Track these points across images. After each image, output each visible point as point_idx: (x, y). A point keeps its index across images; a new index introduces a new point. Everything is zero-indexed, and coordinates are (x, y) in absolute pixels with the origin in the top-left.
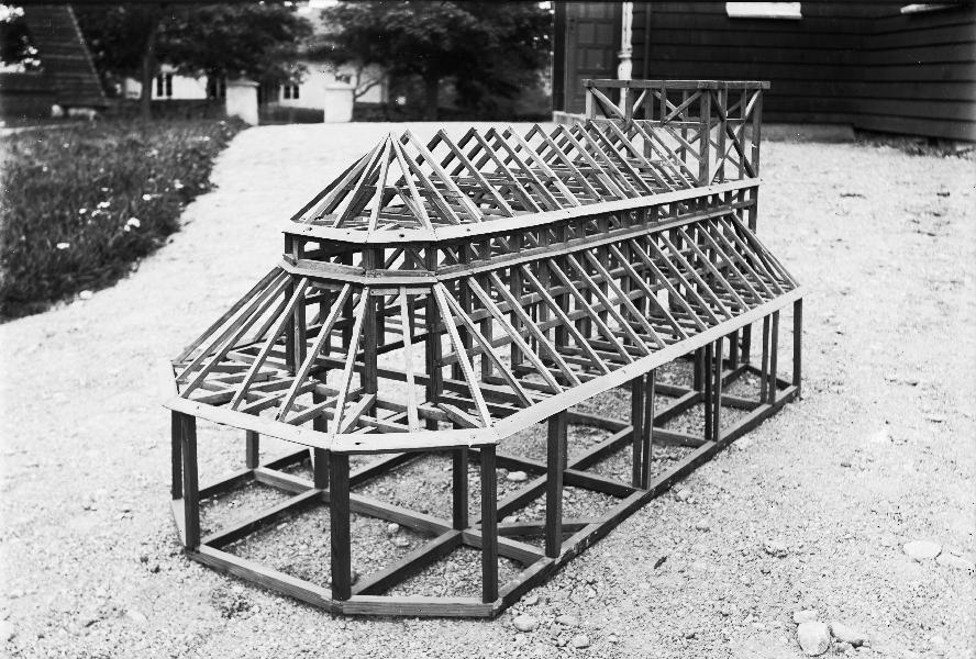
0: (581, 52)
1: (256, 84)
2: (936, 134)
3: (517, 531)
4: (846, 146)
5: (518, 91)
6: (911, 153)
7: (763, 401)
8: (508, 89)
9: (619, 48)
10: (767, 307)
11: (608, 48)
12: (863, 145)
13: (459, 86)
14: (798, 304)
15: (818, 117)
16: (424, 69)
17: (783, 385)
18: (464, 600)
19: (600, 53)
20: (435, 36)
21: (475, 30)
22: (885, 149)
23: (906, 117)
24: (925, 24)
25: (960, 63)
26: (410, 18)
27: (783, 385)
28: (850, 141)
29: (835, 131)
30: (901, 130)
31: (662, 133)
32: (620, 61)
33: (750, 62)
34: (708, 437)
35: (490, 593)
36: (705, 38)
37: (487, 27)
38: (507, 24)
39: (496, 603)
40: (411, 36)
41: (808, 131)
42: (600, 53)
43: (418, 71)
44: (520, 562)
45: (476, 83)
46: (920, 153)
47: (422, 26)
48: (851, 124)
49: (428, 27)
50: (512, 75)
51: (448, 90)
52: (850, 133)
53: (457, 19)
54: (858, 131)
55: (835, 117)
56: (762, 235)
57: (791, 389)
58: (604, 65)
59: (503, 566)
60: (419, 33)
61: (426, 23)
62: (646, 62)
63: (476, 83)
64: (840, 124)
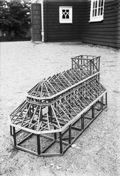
0: (35, 30)
1: (72, 7)
2: (95, 43)
3: (64, 142)
4: (81, 45)
5: (26, 33)
6: (91, 46)
7: (101, 109)
8: (24, 33)
9: (41, 29)
10: (101, 96)
11: (39, 29)
12: (83, 45)
13: (15, 33)
14: (106, 93)
15: (76, 40)
16: (8, 30)
17: (104, 105)
18: (58, 153)
19: (38, 30)
20: (9, 24)
21: (17, 23)
22: (87, 46)
23: (90, 40)
24: (92, 24)
25: (118, 35)
26: (4, 21)
27: (104, 105)
28: (82, 44)
29: (78, 42)
30: (89, 42)
31: (22, 19)
32: (42, 32)
33: (64, 31)
34: (92, 118)
35: (61, 153)
36: (56, 27)
37: (19, 22)
38: (23, 21)
39: (62, 152)
40: (5, 24)
41: (74, 43)
42: (38, 30)
43: (7, 30)
44: (66, 145)
45: (18, 32)
46: (92, 46)
47: (7, 22)
48: (81, 41)
49: (8, 22)
50: (25, 30)
51: (13, 34)
52: (81, 43)
53: (13, 21)
54: (83, 42)
55: (79, 40)
56: (100, 82)
57: (106, 106)
58: (39, 32)
59: (63, 146)
60: (6, 23)
61: (8, 21)
62: (46, 32)
63: (18, 32)
64: (80, 41)
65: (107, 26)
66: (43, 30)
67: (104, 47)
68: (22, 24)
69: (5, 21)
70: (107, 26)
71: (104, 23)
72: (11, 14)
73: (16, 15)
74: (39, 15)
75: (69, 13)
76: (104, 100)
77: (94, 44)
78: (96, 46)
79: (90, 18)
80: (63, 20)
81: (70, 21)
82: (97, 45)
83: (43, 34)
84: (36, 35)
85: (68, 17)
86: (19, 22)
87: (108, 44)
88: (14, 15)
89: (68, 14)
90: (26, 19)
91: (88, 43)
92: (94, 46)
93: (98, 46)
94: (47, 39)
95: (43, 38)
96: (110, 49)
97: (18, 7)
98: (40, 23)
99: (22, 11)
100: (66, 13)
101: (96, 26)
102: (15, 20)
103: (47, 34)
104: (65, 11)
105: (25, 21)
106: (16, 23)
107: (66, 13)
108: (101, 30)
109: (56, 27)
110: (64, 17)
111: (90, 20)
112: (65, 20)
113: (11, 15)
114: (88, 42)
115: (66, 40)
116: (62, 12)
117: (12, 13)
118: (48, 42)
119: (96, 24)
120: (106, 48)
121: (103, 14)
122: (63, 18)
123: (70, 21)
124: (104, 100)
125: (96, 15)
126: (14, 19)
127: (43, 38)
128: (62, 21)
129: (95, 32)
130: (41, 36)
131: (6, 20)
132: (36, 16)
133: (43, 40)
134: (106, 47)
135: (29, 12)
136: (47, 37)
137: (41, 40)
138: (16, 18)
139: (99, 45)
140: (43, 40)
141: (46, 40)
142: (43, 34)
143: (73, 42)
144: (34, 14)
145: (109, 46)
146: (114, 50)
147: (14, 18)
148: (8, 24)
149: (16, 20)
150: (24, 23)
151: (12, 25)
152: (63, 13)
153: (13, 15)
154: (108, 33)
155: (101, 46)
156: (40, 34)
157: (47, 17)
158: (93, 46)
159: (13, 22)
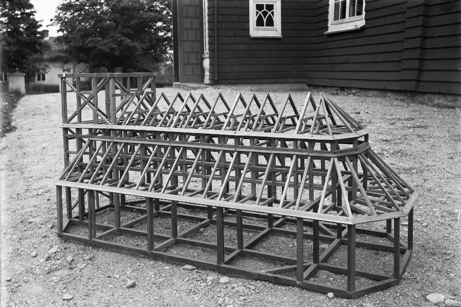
16: (107, 64)
19: (194, 55)
20: (112, 49)
24: (335, 39)
26: (99, 41)
32: (203, 59)
38: (145, 43)
46: (337, 94)
47: (105, 45)
49: (108, 45)
52: (305, 86)
53: (121, 41)
54: (309, 85)
55: (299, 80)
58: (197, 60)
60: (104, 48)
61: (107, 43)
65: (377, 40)
66: (206, 51)
67: (371, 93)
68: (143, 49)
69: (101, 42)
70: (377, 40)
71: (368, 32)
72: (117, 26)
73: (128, 27)
74: (197, 18)
75: (273, 13)
76: (404, 232)
77: (342, 89)
78: (346, 94)
79: (329, 25)
80: (257, 30)
81: (276, 31)
82: (349, 88)
83: (206, 63)
84: (189, 68)
85: (270, 23)
86: (136, 44)
87: (381, 85)
88: (124, 27)
89: (270, 15)
90: (154, 37)
91: (325, 87)
92: (342, 92)
93: (354, 91)
94: (218, 76)
95: (207, 73)
96: (389, 97)
97: (135, 9)
98: (199, 38)
99: (144, 18)
100: (265, 14)
101: (345, 43)
102: (127, 39)
103: (218, 65)
104: (265, 11)
105: (150, 41)
106: (128, 48)
107: (265, 14)
108: (359, 50)
109: (241, 47)
110: (260, 23)
111: (327, 30)
112: (265, 30)
113: (115, 28)
114: (323, 85)
115: (266, 81)
116: (255, 10)
117: (117, 23)
118: (221, 84)
119: (347, 36)
120: (376, 96)
121: (364, 13)
122: (257, 25)
123: (276, 31)
124: (404, 232)
125: (343, 16)
126: (123, 38)
127: (207, 73)
128: (255, 31)
129: (345, 57)
130: (203, 70)
131: (103, 38)
132: (189, 20)
133: (207, 80)
134: (376, 93)
135: (160, 20)
136: (218, 72)
137: (202, 81)
138: (128, 36)
139: (355, 88)
140: (207, 80)
141: (216, 79)
142: (206, 63)
143: (284, 86)
144: (185, 15)
145: (384, 91)
146: (401, 98)
147: (123, 34)
148: (107, 50)
149: (129, 41)
150: (147, 47)
151: (117, 53)
152: (257, 13)
153: (120, 27)
154: (380, 58)
155: (363, 92)
156: (199, 66)
157: (218, 22)
158: (339, 92)
159: (120, 43)
